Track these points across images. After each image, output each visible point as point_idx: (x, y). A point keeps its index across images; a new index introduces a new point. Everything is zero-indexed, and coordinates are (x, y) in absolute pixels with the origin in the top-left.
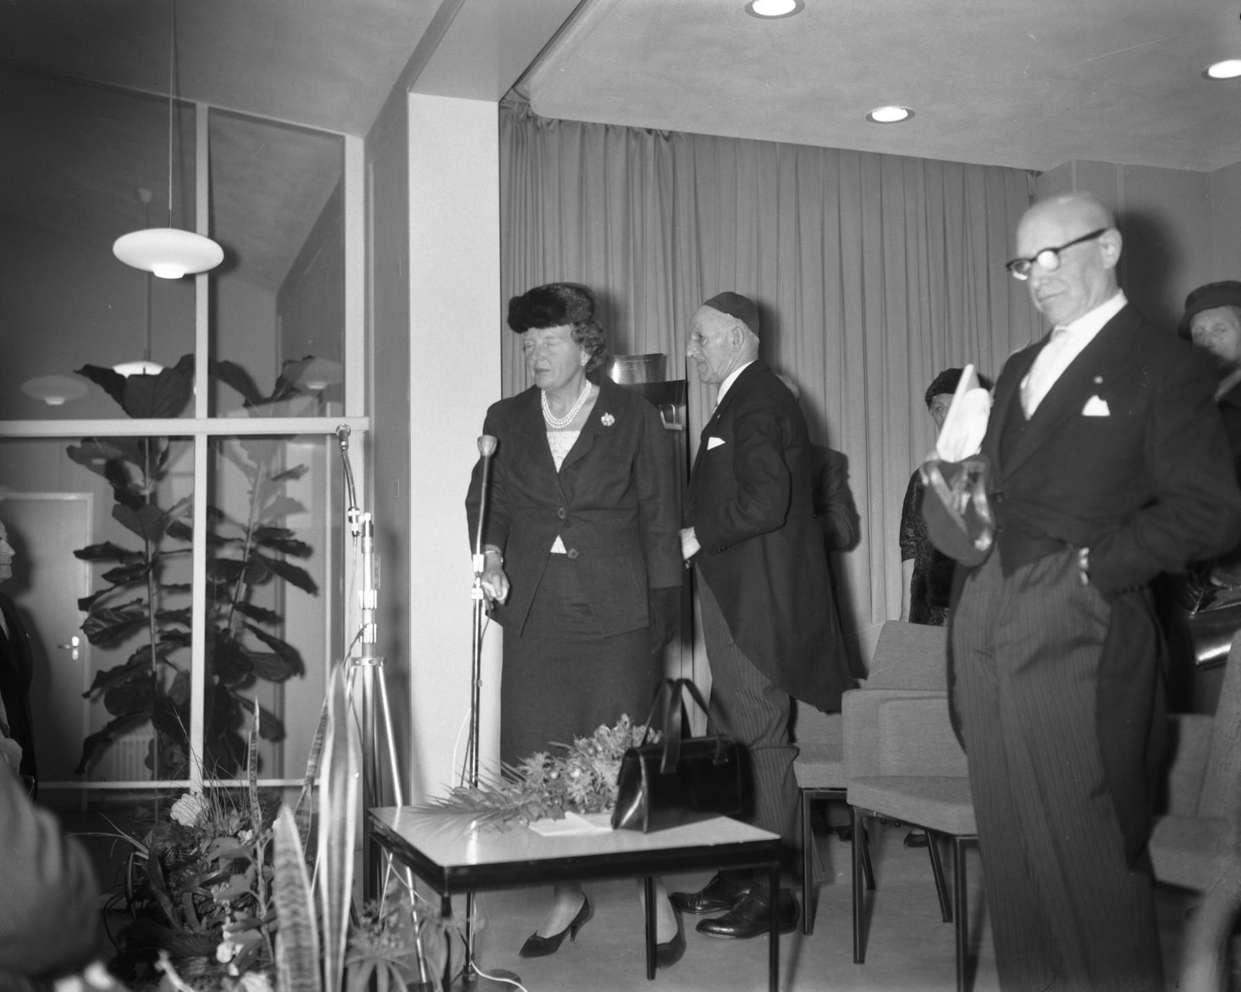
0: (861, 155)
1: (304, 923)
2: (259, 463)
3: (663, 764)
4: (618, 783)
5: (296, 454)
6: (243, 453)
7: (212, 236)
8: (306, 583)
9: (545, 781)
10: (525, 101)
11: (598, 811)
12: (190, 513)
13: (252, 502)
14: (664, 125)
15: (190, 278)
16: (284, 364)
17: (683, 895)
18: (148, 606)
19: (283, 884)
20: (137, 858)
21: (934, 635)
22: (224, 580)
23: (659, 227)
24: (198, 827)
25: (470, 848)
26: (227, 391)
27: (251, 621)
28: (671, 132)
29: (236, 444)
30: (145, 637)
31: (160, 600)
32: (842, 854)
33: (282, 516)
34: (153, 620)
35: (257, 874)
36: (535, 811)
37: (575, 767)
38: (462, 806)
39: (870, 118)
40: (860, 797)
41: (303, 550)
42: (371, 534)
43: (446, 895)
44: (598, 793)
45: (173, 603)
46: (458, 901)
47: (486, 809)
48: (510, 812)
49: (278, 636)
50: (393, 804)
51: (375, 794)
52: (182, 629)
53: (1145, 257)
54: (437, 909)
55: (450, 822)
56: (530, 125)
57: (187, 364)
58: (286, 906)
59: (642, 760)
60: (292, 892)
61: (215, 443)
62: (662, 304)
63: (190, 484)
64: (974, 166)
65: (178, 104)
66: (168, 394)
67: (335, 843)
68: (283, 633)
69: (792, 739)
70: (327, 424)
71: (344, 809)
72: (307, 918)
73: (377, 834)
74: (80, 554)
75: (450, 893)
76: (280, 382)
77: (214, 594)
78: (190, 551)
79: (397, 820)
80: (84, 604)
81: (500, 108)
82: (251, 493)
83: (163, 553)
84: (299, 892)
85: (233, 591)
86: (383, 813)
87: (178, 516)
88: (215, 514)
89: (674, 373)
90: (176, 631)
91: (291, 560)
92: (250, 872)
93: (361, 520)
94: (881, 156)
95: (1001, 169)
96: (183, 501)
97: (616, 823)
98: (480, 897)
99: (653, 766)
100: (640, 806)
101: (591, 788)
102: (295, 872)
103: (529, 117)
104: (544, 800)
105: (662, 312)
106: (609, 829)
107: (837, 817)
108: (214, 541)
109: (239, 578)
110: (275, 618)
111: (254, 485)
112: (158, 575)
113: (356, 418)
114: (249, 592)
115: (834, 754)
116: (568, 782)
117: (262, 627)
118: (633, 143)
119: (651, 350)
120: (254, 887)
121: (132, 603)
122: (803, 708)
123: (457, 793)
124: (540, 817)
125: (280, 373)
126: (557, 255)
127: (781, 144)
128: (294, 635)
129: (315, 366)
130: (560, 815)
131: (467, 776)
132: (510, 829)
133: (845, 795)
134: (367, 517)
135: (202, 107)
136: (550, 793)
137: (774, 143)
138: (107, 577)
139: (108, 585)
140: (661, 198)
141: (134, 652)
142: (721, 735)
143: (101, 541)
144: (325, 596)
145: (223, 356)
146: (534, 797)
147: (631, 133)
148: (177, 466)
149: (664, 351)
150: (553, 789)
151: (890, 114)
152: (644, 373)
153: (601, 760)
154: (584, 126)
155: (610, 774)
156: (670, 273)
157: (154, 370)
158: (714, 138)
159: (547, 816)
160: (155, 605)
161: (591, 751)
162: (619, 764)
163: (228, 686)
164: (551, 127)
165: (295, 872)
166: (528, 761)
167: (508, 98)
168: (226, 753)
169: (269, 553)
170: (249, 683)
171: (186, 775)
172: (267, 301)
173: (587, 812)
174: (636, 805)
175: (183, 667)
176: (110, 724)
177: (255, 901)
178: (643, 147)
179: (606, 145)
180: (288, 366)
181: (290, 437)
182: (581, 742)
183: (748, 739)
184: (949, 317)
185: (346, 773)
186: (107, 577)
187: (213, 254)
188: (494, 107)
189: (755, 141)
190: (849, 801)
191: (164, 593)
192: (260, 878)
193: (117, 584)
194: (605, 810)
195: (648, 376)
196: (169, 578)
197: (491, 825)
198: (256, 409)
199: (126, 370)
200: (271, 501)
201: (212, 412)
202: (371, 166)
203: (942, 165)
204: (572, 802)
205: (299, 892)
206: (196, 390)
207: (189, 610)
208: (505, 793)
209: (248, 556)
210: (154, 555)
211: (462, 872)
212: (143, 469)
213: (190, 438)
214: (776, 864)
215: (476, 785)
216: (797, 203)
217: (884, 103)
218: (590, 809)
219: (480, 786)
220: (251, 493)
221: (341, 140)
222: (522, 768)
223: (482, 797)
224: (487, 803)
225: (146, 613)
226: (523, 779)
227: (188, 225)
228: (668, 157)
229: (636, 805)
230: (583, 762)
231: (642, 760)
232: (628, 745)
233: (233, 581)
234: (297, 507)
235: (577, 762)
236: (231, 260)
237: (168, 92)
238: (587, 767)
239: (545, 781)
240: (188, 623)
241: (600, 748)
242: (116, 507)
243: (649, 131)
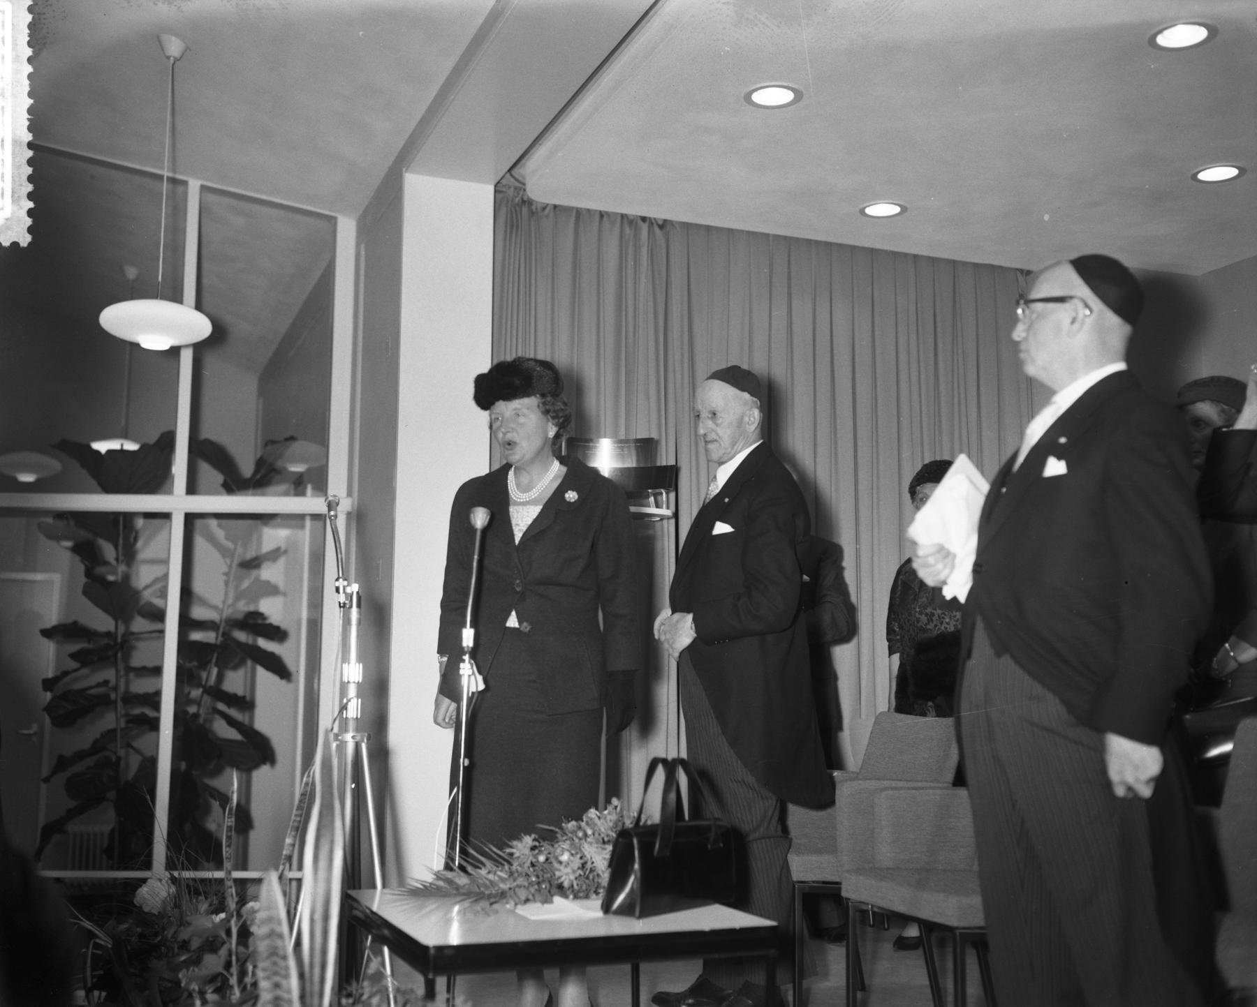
0: (854, 249)
1: (285, 996)
2: (236, 545)
3: (657, 846)
4: (610, 866)
6: (220, 534)
7: (199, 307)
8: (279, 668)
10: (521, 186)
11: (587, 897)
12: (163, 594)
13: (227, 583)
14: (658, 213)
15: (175, 351)
16: (266, 445)
17: (667, 994)
18: (116, 688)
19: (265, 955)
20: (97, 946)
21: (929, 728)
22: (195, 663)
23: (651, 310)
24: (161, 915)
26: (208, 473)
27: (221, 706)
28: (665, 221)
29: (213, 523)
30: (109, 720)
31: (127, 683)
32: (836, 958)
33: (255, 599)
34: (120, 704)
35: (230, 955)
36: (523, 894)
37: (563, 850)
39: (862, 212)
40: (857, 889)
41: (278, 634)
42: (359, 606)
43: (431, 976)
44: (587, 878)
45: (141, 686)
46: (441, 982)
48: (495, 896)
49: (247, 722)
50: (374, 887)
51: (355, 876)
52: (150, 713)
53: (1147, 304)
54: (420, 990)
55: (432, 905)
56: (525, 210)
57: (167, 441)
58: (268, 978)
59: (635, 841)
60: (275, 964)
61: (190, 519)
62: (653, 387)
63: (161, 567)
64: (965, 264)
65: (173, 181)
66: (148, 471)
67: (318, 916)
68: (252, 718)
69: (785, 831)
70: (311, 503)
71: (329, 881)
72: (289, 991)
73: (356, 918)
74: (47, 633)
76: (260, 463)
77: (183, 675)
78: (162, 632)
79: (382, 902)
80: (48, 684)
81: (496, 191)
82: (226, 574)
83: (133, 634)
84: (282, 963)
85: (204, 675)
86: (362, 895)
87: (148, 596)
88: (187, 594)
89: (665, 458)
90: (144, 714)
91: (262, 643)
92: (223, 952)
94: (872, 252)
95: (992, 267)
96: (156, 580)
97: (606, 908)
98: (461, 981)
100: (632, 890)
101: (580, 872)
102: (279, 943)
103: (524, 202)
104: (531, 884)
105: (653, 399)
106: (600, 914)
107: (830, 917)
108: (186, 622)
109: (210, 661)
110: (246, 703)
111: (230, 567)
112: (127, 657)
114: (220, 677)
115: (829, 846)
116: (556, 865)
117: (233, 712)
118: (627, 231)
119: (642, 435)
120: (228, 965)
121: (98, 685)
122: (792, 808)
124: (527, 901)
125: (258, 456)
126: (549, 337)
127: (775, 236)
128: (263, 722)
129: (297, 447)
130: (547, 900)
132: (497, 912)
133: (840, 889)
134: (355, 588)
135: (194, 186)
136: (538, 877)
137: (768, 235)
138: (73, 656)
139: (74, 665)
140: (654, 288)
141: (98, 736)
142: (717, 819)
143: (70, 621)
144: (298, 681)
145: (207, 433)
146: (521, 881)
147: (625, 221)
148: (146, 550)
149: (654, 435)
152: (634, 458)
153: (591, 843)
154: (579, 213)
155: (600, 858)
157: (131, 446)
159: (535, 901)
160: (122, 688)
161: (580, 834)
162: (610, 848)
163: (195, 773)
164: (546, 211)
165: (279, 943)
166: (515, 843)
167: (504, 182)
168: (193, 842)
169: (241, 636)
170: (217, 772)
171: (148, 865)
173: (576, 897)
175: (148, 754)
176: (69, 811)
177: (225, 981)
178: (637, 231)
179: (600, 231)
180: (269, 448)
182: (572, 825)
183: (745, 827)
184: (940, 421)
185: (332, 842)
186: (73, 656)
187: (201, 327)
188: (490, 189)
189: (748, 232)
190: (844, 894)
191: (132, 675)
192: (234, 958)
193: (84, 664)
194: (594, 896)
195: (638, 460)
196: (138, 660)
199: (102, 446)
201: (192, 489)
202: (363, 246)
205: (282, 963)
206: (174, 470)
207: (158, 694)
208: (491, 877)
209: (220, 638)
210: (123, 635)
212: (116, 548)
213: (166, 516)
214: (772, 952)
216: (790, 295)
217: (877, 198)
218: (579, 894)
220: (226, 574)
221: (332, 221)
222: (508, 850)
225: (113, 696)
226: (510, 864)
227: (176, 296)
228: (663, 246)
230: (571, 845)
231: (635, 841)
232: (619, 828)
233: (204, 665)
235: (566, 845)
236: (219, 334)
237: (162, 168)
238: (576, 850)
239: (533, 865)
240: (157, 706)
241: (589, 832)
242: (86, 585)
243: (644, 219)
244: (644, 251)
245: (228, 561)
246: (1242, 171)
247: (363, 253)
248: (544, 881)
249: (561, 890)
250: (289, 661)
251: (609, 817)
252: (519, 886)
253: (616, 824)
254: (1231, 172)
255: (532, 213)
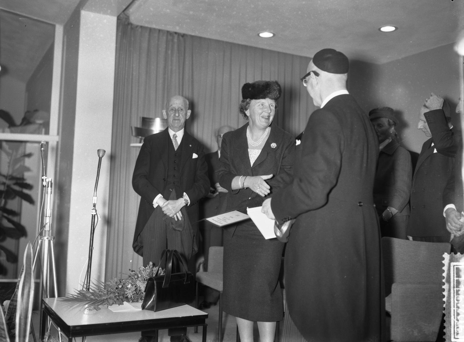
5: (29, 148)
8: (30, 200)
9: (116, 288)
10: (128, 18)
11: (137, 301)
13: (9, 166)
25: (82, 316)
38: (82, 298)
41: (29, 187)
42: (51, 187)
47: (92, 300)
49: (18, 221)
75: (72, 337)
79: (54, 304)
91: (26, 191)
93: (47, 180)
97: (143, 307)
99: (159, 284)
100: (153, 300)
106: (141, 309)
110: (17, 214)
111: (10, 160)
113: (53, 138)
114: (6, 203)
117: (10, 217)
123: (80, 293)
124: (113, 303)
129: (40, 114)
131: (85, 286)
132: (100, 309)
136: (118, 293)
150: (119, 292)
151: (266, 35)
154: (151, 30)
155: (142, 286)
156: (181, 88)
158: (201, 38)
159: (116, 304)
161: (136, 277)
162: (146, 282)
164: (138, 28)
165: (3, 332)
169: (17, 188)
172: (21, 86)
173: (133, 301)
174: (152, 300)
181: (26, 142)
194: (140, 301)
197: (92, 307)
198: (13, 129)
200: (18, 166)
202: (66, 36)
203: (285, 54)
204: (127, 297)
209: (6, 188)
211: (77, 328)
215: (89, 290)
217: (264, 30)
218: (133, 300)
219: (90, 290)
221: (54, 26)
223: (91, 295)
224: (92, 297)
229: (152, 300)
234: (28, 170)
239: (116, 288)
241: (140, 276)
243: (176, 33)
244: (176, 46)
245: (10, 157)
246: (396, 28)
247: (65, 40)
248: (121, 295)
249: (127, 299)
250: (34, 197)
251: (147, 270)
252: (110, 298)
253: (150, 274)
254: (392, 29)
255: (132, 28)
